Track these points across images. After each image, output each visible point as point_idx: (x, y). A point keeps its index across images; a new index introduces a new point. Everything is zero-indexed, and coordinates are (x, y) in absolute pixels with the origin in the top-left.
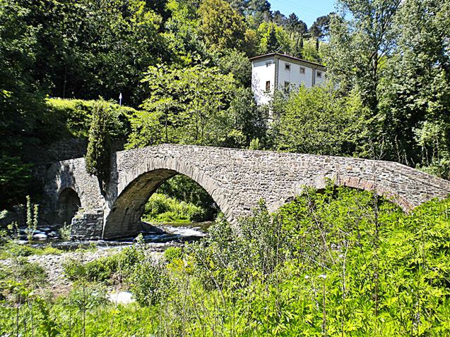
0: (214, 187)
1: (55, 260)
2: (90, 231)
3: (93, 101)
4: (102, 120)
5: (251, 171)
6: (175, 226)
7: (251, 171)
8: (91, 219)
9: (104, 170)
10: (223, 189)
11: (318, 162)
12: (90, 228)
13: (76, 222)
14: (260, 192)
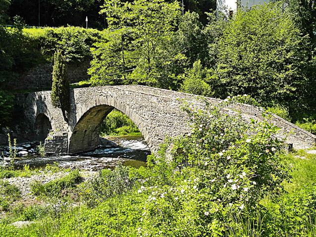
0: (140, 121)
1: (26, 182)
2: (59, 149)
3: (62, 28)
4: (61, 64)
5: (162, 112)
6: (129, 139)
7: (162, 112)
8: (59, 139)
9: (66, 103)
10: (145, 124)
11: (202, 110)
12: (58, 147)
13: (48, 142)
14: (168, 128)
